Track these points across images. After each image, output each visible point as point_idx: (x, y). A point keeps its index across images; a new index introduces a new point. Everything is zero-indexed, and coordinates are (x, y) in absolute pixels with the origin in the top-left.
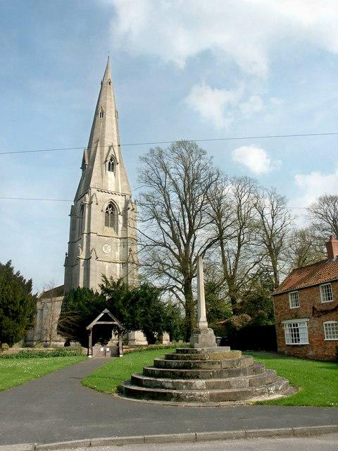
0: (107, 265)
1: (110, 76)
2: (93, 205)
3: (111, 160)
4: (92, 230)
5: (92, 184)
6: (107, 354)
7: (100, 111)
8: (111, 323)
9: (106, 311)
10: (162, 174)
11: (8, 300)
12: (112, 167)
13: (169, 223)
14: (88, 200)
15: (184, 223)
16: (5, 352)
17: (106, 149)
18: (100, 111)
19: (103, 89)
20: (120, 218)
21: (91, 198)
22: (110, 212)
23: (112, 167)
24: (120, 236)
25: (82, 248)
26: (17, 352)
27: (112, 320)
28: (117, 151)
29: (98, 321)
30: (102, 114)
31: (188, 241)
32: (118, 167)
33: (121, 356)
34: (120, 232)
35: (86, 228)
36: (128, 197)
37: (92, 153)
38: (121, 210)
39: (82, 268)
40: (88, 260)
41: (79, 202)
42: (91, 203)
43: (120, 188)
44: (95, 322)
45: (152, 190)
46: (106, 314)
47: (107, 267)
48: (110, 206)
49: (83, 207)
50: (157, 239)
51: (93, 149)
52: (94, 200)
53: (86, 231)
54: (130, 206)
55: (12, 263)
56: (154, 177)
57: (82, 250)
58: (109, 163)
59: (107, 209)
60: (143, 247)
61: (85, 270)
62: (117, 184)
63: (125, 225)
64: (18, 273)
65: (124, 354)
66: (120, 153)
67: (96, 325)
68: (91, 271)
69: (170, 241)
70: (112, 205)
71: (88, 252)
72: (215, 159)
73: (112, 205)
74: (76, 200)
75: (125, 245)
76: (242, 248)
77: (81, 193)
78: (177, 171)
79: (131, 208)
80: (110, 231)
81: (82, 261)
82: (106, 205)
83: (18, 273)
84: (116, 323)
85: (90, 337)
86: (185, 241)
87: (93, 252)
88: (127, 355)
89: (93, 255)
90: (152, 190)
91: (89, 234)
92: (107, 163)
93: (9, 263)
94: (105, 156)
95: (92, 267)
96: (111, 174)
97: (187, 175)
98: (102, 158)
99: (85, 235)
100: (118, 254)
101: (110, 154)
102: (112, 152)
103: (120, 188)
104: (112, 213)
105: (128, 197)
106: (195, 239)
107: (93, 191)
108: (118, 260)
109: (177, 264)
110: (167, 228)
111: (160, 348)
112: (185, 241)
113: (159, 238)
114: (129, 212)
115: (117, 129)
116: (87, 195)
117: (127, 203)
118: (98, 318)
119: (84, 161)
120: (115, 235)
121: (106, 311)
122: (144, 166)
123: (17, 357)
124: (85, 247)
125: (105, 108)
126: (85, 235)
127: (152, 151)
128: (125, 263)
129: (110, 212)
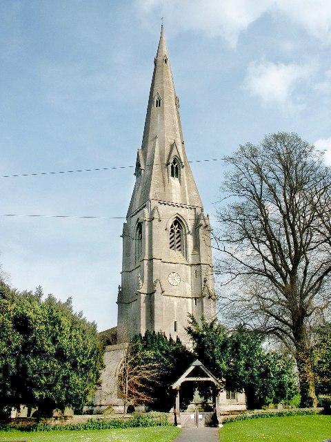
0: (176, 301)
1: (165, 50)
2: (155, 222)
3: (174, 162)
4: (155, 254)
5: (151, 196)
6: (200, 422)
7: (156, 99)
8: (205, 379)
9: (197, 363)
10: (256, 178)
11: (77, 350)
12: (175, 172)
13: (268, 242)
14: (147, 216)
15: (289, 243)
16: (69, 421)
17: (167, 148)
18: (156, 99)
19: (159, 70)
20: (190, 239)
21: (152, 213)
22: (176, 231)
23: (175, 172)
24: (190, 261)
25: (142, 279)
26: (85, 422)
27: (208, 377)
28: (180, 151)
29: (187, 377)
30: (159, 103)
31: (295, 267)
32: (183, 171)
33: (221, 426)
34: (190, 257)
35: (147, 252)
36: (198, 210)
37: (149, 154)
38: (191, 228)
39: (143, 305)
40: (151, 295)
41: (134, 219)
42: (152, 219)
43: (188, 198)
44: (183, 379)
45: (244, 200)
46: (197, 367)
47: (175, 304)
48: (176, 222)
49: (140, 226)
50: (252, 264)
51: (149, 148)
52: (156, 215)
53: (147, 257)
54: (202, 222)
55: (73, 300)
56: (245, 182)
57: (143, 282)
58: (172, 167)
59: (172, 227)
60: (234, 276)
61: (147, 308)
62: (183, 194)
63: (197, 246)
64: (81, 315)
65: (223, 423)
66: (184, 153)
67: (186, 382)
68: (156, 310)
69: (270, 267)
70: (178, 222)
71: (151, 285)
72: (305, 150)
73: (178, 222)
74: (129, 216)
75: (198, 274)
76: (309, 265)
77: (137, 206)
78: (275, 172)
79: (204, 225)
80: (176, 255)
81: (143, 296)
82: (171, 222)
83: (81, 315)
84: (211, 379)
85: (178, 399)
86: (291, 266)
87: (158, 284)
88: (226, 424)
89: (158, 289)
90: (244, 200)
91: (151, 260)
92: (170, 166)
93: (69, 301)
94: (166, 158)
95: (157, 303)
96: (174, 181)
97: (288, 177)
98: (162, 159)
99: (146, 262)
100: (188, 289)
101: (173, 155)
102: (174, 153)
103: (188, 198)
104: (178, 232)
105: (198, 210)
106: (307, 263)
107: (154, 203)
108: (189, 294)
109: (283, 298)
110: (268, 253)
111: (271, 416)
112: (291, 266)
113: (257, 263)
114: (201, 230)
115: (179, 122)
116: (146, 210)
117: (197, 219)
118: (205, 379)
119: (138, 165)
120: (183, 260)
121: (197, 363)
122: (231, 169)
123: (85, 428)
124: (146, 278)
125: (163, 93)
126: (146, 262)
127: (242, 149)
128: (198, 299)
129: (176, 231)
